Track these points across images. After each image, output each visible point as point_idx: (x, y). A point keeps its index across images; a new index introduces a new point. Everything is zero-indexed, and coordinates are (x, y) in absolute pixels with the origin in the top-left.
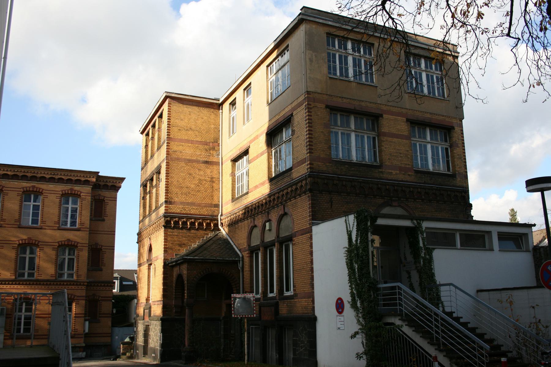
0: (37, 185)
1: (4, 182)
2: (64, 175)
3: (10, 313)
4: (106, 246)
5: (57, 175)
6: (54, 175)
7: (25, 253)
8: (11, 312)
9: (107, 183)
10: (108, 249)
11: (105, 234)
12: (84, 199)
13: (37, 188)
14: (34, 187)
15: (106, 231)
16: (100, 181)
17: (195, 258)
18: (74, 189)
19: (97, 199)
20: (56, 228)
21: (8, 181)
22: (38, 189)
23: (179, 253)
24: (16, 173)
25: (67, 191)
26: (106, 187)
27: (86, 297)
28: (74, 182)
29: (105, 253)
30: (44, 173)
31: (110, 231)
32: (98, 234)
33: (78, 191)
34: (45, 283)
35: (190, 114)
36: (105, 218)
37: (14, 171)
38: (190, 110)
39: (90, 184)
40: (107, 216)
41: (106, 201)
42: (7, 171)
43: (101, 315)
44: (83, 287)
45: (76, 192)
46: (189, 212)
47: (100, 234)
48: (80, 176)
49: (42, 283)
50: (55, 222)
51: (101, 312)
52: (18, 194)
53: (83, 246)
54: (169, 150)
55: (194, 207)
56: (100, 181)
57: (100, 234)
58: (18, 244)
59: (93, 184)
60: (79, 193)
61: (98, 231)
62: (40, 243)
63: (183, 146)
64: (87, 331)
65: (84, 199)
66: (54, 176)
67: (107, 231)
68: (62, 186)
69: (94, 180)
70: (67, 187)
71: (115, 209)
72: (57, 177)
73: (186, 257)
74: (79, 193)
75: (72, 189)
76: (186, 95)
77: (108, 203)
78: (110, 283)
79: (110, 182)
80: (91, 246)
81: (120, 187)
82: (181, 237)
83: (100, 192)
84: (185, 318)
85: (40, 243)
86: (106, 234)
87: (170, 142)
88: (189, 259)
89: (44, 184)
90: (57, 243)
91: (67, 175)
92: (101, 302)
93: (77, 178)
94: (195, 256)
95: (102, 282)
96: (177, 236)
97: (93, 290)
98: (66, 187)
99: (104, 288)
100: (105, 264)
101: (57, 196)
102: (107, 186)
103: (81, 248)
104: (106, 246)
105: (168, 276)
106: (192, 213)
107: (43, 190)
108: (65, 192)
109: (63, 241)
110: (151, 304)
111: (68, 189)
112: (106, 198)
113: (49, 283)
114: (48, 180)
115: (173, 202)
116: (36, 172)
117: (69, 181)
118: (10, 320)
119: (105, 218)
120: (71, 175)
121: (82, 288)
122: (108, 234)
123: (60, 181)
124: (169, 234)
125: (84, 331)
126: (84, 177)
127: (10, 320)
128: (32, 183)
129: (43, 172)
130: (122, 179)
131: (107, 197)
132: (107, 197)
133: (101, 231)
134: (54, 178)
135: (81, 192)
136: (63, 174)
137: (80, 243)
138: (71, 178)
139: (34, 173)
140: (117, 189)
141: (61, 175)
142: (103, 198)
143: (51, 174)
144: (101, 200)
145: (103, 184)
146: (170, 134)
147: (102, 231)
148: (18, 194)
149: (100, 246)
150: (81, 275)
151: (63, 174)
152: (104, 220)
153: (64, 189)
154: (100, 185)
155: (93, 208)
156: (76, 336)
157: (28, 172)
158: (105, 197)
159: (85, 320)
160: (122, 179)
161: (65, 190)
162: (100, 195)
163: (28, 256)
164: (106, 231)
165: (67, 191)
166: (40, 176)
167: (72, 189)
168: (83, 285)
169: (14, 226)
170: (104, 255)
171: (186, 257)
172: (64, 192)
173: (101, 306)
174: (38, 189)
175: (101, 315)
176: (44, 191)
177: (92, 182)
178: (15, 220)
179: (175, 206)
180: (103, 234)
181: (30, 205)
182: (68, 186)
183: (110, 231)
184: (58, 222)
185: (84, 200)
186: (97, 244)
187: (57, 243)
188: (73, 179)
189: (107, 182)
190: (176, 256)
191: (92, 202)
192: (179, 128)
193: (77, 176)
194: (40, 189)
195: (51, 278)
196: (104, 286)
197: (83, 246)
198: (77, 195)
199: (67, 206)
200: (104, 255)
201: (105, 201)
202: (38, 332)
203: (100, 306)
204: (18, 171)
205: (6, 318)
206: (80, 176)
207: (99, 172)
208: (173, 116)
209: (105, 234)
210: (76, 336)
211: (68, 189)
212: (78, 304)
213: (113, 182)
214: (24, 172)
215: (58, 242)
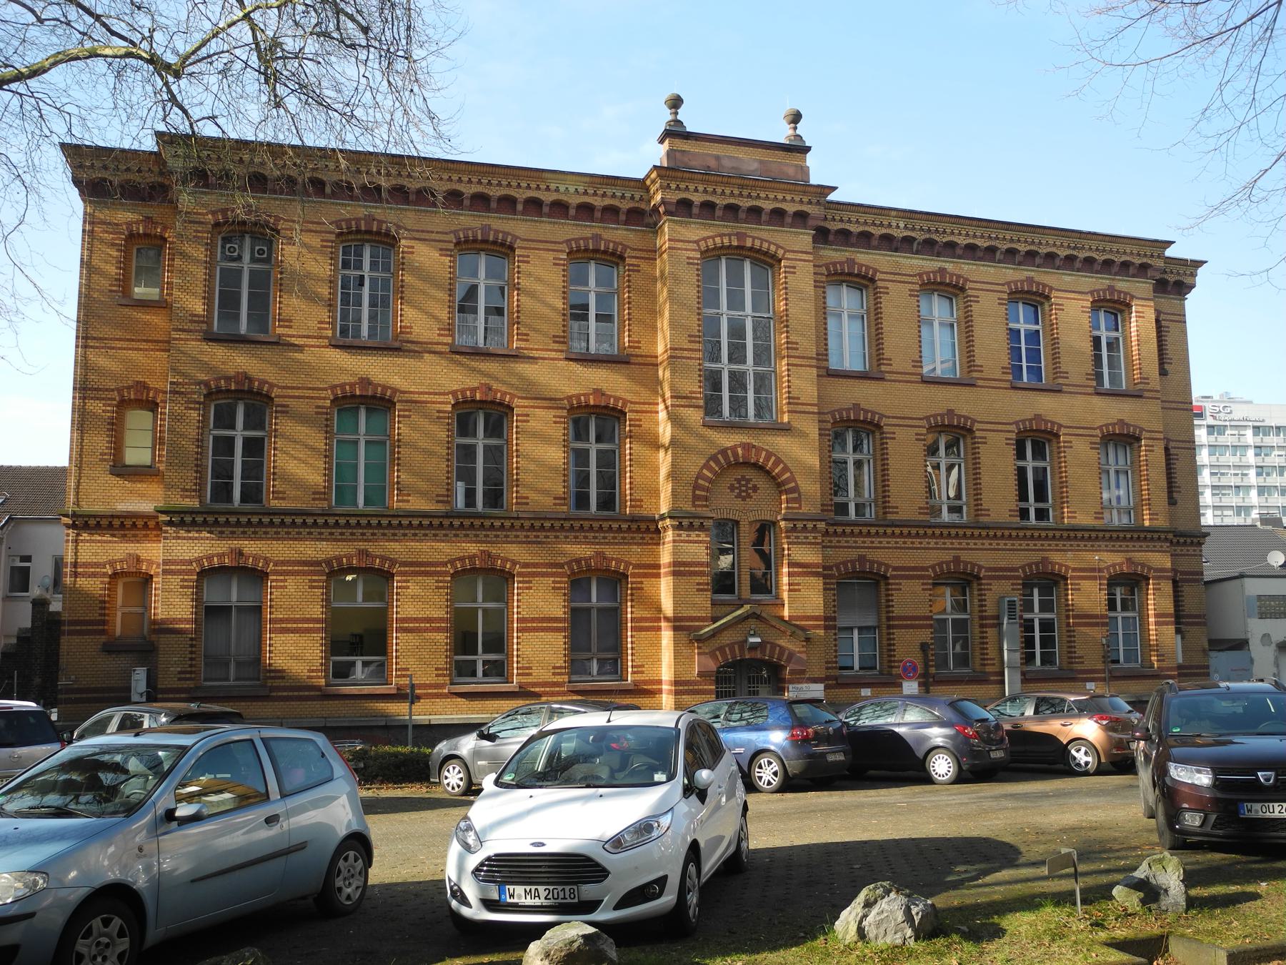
1: (966, 267)
5: (1083, 248)
9: (1166, 276)
13: (1038, 284)
18: (1117, 288)
28: (622, 217)
30: (1054, 245)
42: (975, 236)
58: (332, 398)
66: (1075, 253)
70: (1102, 283)
71: (1187, 344)
78: (1197, 537)
81: (1192, 286)
91: (1104, 251)
98: (470, 221)
103: (526, 411)
120: (1111, 251)
121: (936, 543)
128: (1027, 270)
130: (1200, 263)
137: (279, 387)
138: (1113, 258)
139: (1033, 243)
154: (378, 188)
160: (1200, 263)
163: (480, 442)
166: (1045, 251)
176: (1054, 294)
194: (1044, 286)
195: (922, 517)
206: (1132, 253)
211: (1024, 278)
212: (1159, 589)
214: (1012, 240)
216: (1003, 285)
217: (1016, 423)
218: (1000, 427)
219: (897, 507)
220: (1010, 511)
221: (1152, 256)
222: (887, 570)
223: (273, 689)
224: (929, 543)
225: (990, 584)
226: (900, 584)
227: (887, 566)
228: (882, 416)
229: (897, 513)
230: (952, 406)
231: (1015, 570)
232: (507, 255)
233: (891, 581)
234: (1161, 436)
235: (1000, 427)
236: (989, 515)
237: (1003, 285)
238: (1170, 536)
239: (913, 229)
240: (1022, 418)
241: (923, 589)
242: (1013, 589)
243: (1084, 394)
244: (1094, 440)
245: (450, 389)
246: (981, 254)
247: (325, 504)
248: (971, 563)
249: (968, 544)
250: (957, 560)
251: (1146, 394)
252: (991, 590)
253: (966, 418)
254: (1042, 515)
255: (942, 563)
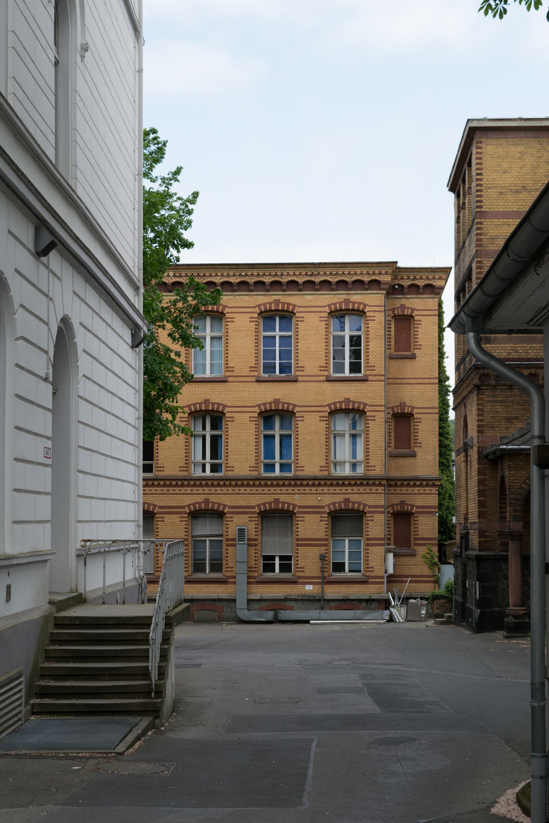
0: (283, 299)
2: (331, 274)
3: (255, 537)
4: (420, 408)
5: (319, 274)
6: (312, 275)
7: (272, 428)
8: (256, 535)
9: (416, 282)
10: (425, 413)
11: (417, 384)
12: (372, 318)
13: (283, 304)
14: (277, 302)
15: (419, 378)
16: (402, 278)
17: (521, 447)
18: (352, 300)
19: (399, 315)
20: (324, 378)
21: (232, 295)
22: (286, 305)
23: (506, 435)
24: (243, 279)
25: (338, 305)
26: (414, 289)
27: (388, 507)
29: (420, 422)
30: (294, 274)
31: (428, 378)
32: (405, 384)
33: (359, 304)
34: (311, 483)
35: (520, 158)
36: (416, 351)
37: (240, 275)
38: (520, 148)
39: (382, 286)
40: (420, 349)
41: (416, 318)
42: (228, 276)
43: (417, 542)
44: (380, 489)
45: (356, 305)
46: (524, 355)
47: (408, 384)
48: (361, 273)
49: (305, 483)
50: (320, 367)
51: (418, 535)
52: (250, 318)
53: (376, 411)
54: (482, 237)
55: (534, 345)
56: (402, 278)
57: (408, 384)
59: (387, 287)
60: (361, 307)
61: (403, 379)
62: (297, 409)
63: (509, 225)
64: (391, 571)
65: (372, 318)
66: (312, 279)
67: (421, 378)
68: (329, 296)
69: (388, 278)
72: (317, 280)
73: (504, 447)
74: (361, 307)
75: (347, 301)
76: (510, 120)
77: (420, 321)
79: (421, 278)
80: (393, 408)
82: (511, 404)
83: (403, 301)
84: (508, 555)
85: (297, 409)
86: (420, 384)
87: (483, 220)
88: (510, 449)
89: (296, 295)
90: (327, 407)
91: (337, 274)
92: (418, 517)
93: (355, 278)
94: (524, 444)
95: (417, 479)
96: (502, 402)
97: (400, 494)
99: (422, 490)
100: (421, 443)
101: (320, 317)
102: (417, 286)
104: (420, 408)
105: (487, 477)
106: (530, 357)
107: (294, 306)
108: (336, 307)
109: (338, 402)
110: (469, 528)
111: (339, 300)
112: (415, 311)
113: (317, 482)
114: (302, 287)
115: (492, 338)
116: (279, 273)
117: (342, 284)
118: (256, 550)
119: (416, 351)
122: (423, 384)
123: (326, 285)
124: (487, 399)
125: (386, 571)
126: (368, 274)
127: (256, 550)
128: (275, 295)
129: (291, 273)
131: (417, 310)
132: (417, 310)
133: (409, 378)
134: (312, 282)
135: (365, 305)
136: (328, 273)
139: (276, 275)
140: (436, 291)
141: (325, 274)
142: (409, 312)
143: (306, 274)
144: (407, 315)
145: (409, 283)
146: (482, 204)
147: (412, 379)
148: (250, 318)
149: (410, 408)
150: (374, 466)
151: (328, 273)
152: (413, 357)
153: (334, 302)
155: (393, 333)
156: (371, 580)
157: (264, 275)
158: (413, 310)
159: (390, 551)
161: (335, 304)
162: (403, 307)
163: (277, 432)
164: (419, 378)
165: (338, 305)
166: (286, 280)
167: (347, 301)
168: (380, 485)
169: (249, 379)
170: (418, 425)
171: (504, 447)
172: (333, 307)
173: (418, 524)
174: (286, 305)
175: (417, 542)
177: (386, 283)
178: (250, 367)
179: (496, 345)
180: (414, 384)
181: (274, 337)
182: (339, 294)
183: (428, 378)
184: (326, 368)
185: (371, 320)
186: (403, 405)
187: (327, 407)
188: (348, 280)
189: (415, 278)
190: (501, 440)
191: (390, 321)
192: (499, 191)
193: (355, 274)
194: (289, 304)
196: (421, 485)
197: (376, 411)
198: (358, 310)
199: (341, 333)
200: (418, 425)
201: (413, 317)
202: (304, 571)
203: (415, 528)
204: (246, 275)
205: (249, 545)
206: (361, 273)
207: (396, 262)
208: (488, 166)
209: (417, 384)
210: (371, 580)
211: (272, 301)
213: (428, 278)
214: (258, 275)
215: (329, 405)
216: (254, 307)
217: (259, 406)
218: (245, 409)
219: (163, 467)
220: (250, 467)
221: (380, 273)
222: (224, 508)
223: (299, 577)
224: (186, 490)
225: (232, 517)
226: (164, 517)
227: (155, 506)
228: (295, 406)
229: (163, 471)
230: (208, 397)
231: (253, 507)
232: (362, 316)
233: (157, 516)
234: (383, 408)
235: (245, 409)
236: (233, 471)
237: (254, 307)
238: (384, 482)
239: (180, 276)
240: (264, 402)
241: (181, 521)
242: (250, 521)
243: (317, 381)
244: (252, 415)
245: (257, 404)
246: (366, 286)
247: (256, 473)
248: (217, 503)
249: (216, 490)
250: (207, 501)
251: (230, 379)
252: (232, 521)
253: (219, 404)
254: (284, 467)
255: (196, 503)
